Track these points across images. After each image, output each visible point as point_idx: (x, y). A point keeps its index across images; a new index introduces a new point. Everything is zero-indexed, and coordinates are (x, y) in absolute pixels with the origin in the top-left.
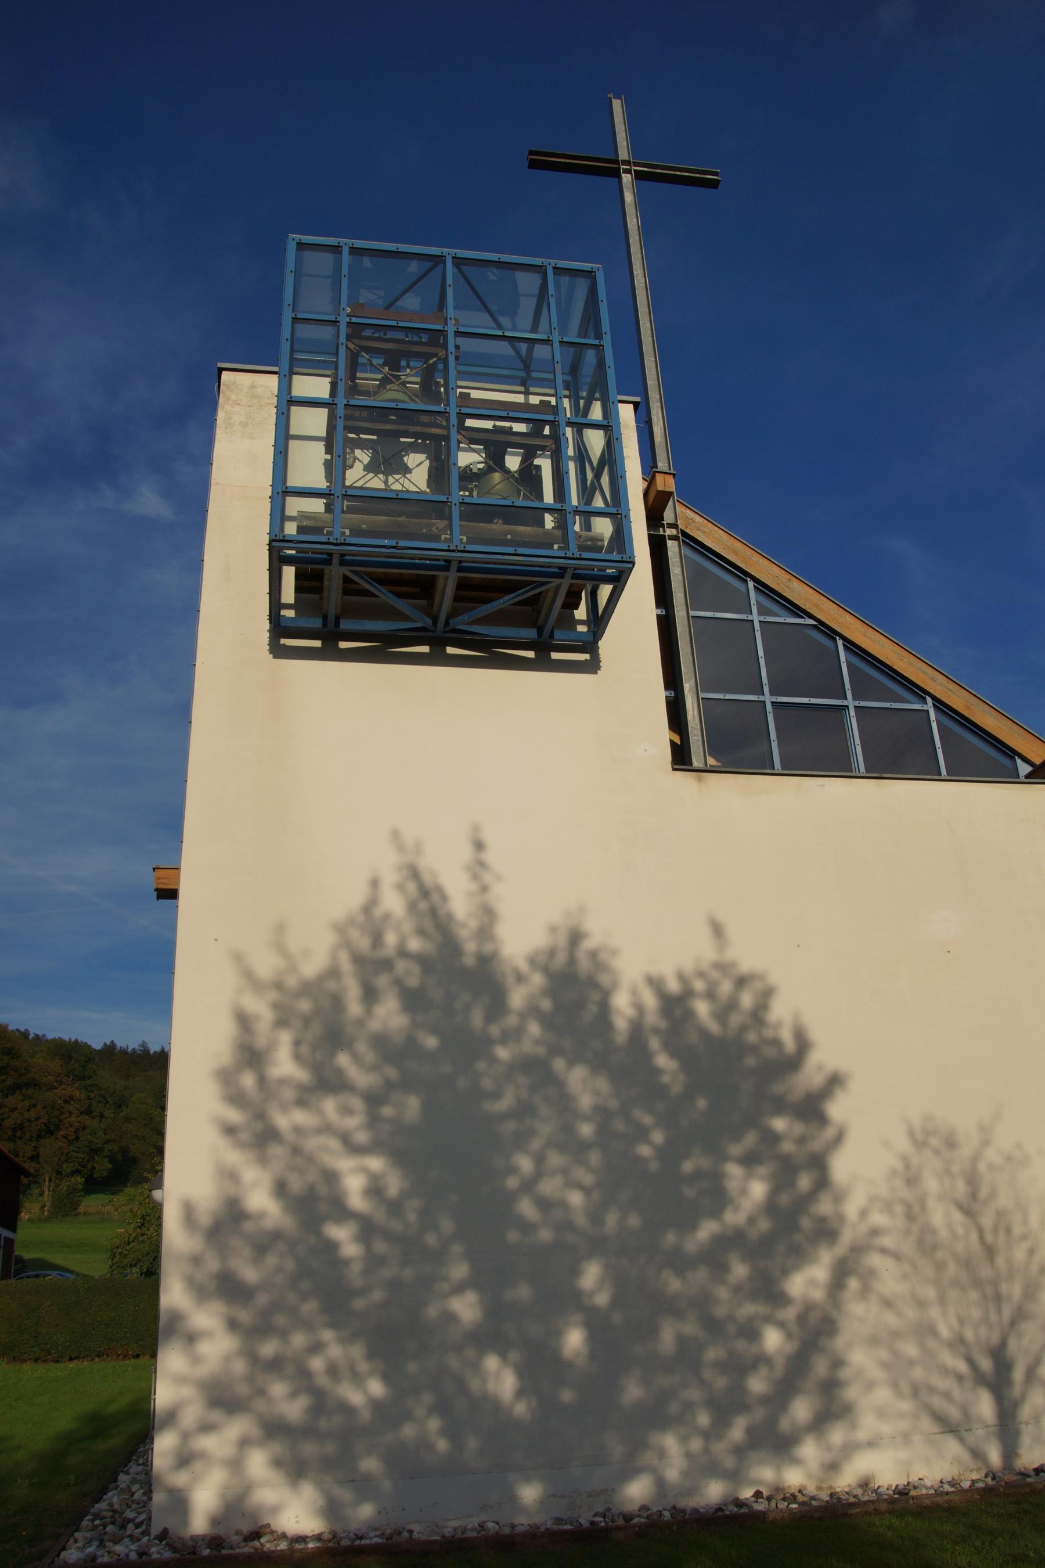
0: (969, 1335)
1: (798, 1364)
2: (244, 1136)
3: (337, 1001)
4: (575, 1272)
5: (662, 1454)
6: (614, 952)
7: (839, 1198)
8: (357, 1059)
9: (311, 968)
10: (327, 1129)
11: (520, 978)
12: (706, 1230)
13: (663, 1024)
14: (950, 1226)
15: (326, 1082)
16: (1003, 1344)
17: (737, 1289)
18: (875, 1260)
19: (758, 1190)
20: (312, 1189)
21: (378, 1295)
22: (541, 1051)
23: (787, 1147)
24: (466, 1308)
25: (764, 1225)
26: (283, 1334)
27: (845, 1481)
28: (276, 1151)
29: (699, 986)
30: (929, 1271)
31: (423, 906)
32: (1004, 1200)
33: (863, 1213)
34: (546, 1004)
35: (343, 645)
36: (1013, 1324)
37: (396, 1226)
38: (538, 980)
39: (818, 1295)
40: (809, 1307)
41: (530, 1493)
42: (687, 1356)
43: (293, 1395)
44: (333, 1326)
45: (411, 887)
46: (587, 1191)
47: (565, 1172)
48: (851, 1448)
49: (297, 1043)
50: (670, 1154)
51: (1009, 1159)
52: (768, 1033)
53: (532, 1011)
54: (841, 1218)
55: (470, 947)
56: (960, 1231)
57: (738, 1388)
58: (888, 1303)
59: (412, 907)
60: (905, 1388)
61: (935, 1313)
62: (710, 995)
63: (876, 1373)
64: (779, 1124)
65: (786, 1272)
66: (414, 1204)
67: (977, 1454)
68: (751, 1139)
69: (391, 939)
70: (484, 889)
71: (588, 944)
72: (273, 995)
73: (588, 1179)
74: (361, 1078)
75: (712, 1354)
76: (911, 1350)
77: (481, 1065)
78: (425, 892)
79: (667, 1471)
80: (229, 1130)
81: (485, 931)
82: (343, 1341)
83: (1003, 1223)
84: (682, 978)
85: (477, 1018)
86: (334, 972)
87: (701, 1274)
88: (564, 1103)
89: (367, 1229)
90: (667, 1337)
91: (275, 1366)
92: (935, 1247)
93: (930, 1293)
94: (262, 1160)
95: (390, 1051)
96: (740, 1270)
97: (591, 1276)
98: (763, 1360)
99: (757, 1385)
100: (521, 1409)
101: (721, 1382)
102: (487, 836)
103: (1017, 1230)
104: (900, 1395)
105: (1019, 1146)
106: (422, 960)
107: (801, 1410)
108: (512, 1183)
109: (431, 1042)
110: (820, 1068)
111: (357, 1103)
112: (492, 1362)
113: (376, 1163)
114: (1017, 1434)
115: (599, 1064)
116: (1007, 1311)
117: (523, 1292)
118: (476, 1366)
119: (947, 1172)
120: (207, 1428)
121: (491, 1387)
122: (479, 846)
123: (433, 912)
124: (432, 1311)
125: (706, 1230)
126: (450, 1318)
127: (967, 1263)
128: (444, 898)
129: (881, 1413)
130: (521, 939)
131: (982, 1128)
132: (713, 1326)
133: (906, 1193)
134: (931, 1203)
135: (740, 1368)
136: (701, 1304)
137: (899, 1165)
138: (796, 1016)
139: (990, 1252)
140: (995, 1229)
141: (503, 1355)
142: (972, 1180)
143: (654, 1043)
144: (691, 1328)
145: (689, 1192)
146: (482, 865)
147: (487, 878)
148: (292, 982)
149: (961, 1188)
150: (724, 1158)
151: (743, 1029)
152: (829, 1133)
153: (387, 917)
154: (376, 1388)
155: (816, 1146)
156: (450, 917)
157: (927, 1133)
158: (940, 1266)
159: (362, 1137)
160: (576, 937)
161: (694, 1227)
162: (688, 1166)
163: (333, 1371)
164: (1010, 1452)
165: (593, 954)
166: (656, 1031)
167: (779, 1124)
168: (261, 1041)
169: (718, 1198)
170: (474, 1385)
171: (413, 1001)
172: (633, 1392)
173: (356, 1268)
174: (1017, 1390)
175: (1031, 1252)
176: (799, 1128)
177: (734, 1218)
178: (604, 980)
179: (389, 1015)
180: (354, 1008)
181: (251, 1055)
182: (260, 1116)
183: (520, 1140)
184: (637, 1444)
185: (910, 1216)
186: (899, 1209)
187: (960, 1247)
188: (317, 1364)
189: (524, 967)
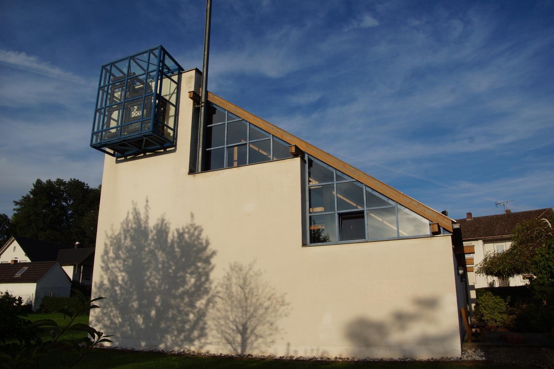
0: (237, 320)
1: (196, 322)
2: (104, 269)
3: (120, 239)
4: (155, 298)
5: (167, 339)
6: (170, 224)
7: (211, 283)
8: (122, 253)
9: (116, 233)
10: (117, 267)
11: (152, 232)
12: (181, 290)
13: (178, 241)
14: (237, 292)
15: (117, 257)
16: (246, 323)
17: (185, 304)
18: (217, 299)
19: (193, 280)
20: (113, 279)
21: (122, 301)
22: (154, 248)
23: (200, 270)
24: (135, 304)
25: (193, 289)
26: (107, 308)
27: (203, 351)
28: (109, 272)
29: (186, 230)
30: (229, 303)
31: (136, 217)
32: (253, 285)
33: (216, 287)
34: (155, 237)
35: (128, 157)
36: (249, 318)
37: (126, 287)
38: (155, 231)
39: (203, 307)
40: (200, 309)
41: (143, 344)
42: (174, 318)
43: (108, 320)
44: (115, 307)
45: (134, 213)
46: (159, 280)
47: (155, 276)
48: (206, 344)
49: (113, 249)
50: (176, 272)
51: (256, 274)
52: (200, 241)
53: (153, 239)
54: (211, 288)
55: (143, 225)
56: (239, 293)
57: (183, 327)
58: (218, 310)
59: (134, 218)
60: (220, 331)
61: (229, 313)
62: (188, 233)
63: (213, 327)
64: (199, 264)
65: (196, 301)
66: (129, 282)
67: (235, 350)
68: (193, 268)
69: (130, 225)
70: (147, 211)
71: (165, 222)
72: (110, 239)
73: (159, 277)
74: (123, 256)
75: (179, 318)
76: (222, 322)
77: (143, 252)
78: (137, 214)
79: (168, 343)
80: (102, 268)
81: (146, 222)
82: (116, 310)
83: (251, 292)
84: (183, 229)
85: (143, 241)
86: (120, 234)
87: (178, 300)
88: (156, 259)
89: (121, 288)
90: (170, 314)
91: (105, 314)
92: (232, 297)
93: (229, 308)
94: (107, 274)
95: (129, 250)
96: (186, 300)
97: (158, 299)
98: (189, 321)
99: (187, 326)
100: (143, 327)
101: (180, 325)
102: (149, 199)
103: (255, 294)
104: (218, 333)
105: (259, 270)
106: (135, 229)
107: (196, 333)
108: (146, 278)
109: (135, 247)
110: (211, 250)
111: (122, 261)
112: (139, 316)
113: (123, 274)
114: (246, 346)
115: (164, 251)
116: (248, 315)
117: (145, 302)
118: (136, 317)
119: (239, 277)
120: (96, 325)
121: (138, 321)
122: (147, 201)
123: (138, 218)
124: (130, 305)
125: (181, 290)
126: (133, 306)
127: (240, 302)
128: (140, 215)
129: (213, 337)
130: (152, 223)
131: (250, 265)
132: (180, 312)
133: (227, 283)
134: (233, 285)
135: (184, 322)
136: (178, 307)
137: (226, 275)
138: (207, 236)
139: (246, 299)
140: (249, 293)
141: (140, 315)
142: (245, 279)
143: (176, 245)
144: (175, 312)
145: (178, 281)
146: (147, 205)
147: (148, 209)
148: (113, 236)
149: (242, 281)
150: (187, 273)
151: (195, 240)
152: (211, 266)
153: (130, 220)
154: (120, 320)
155: (207, 270)
156: (140, 219)
157: (235, 266)
158: (233, 302)
159: (122, 268)
160: (163, 220)
161: (178, 289)
162: (179, 275)
163: (114, 316)
164: (243, 350)
165: (166, 224)
166: (176, 242)
167: (199, 264)
168: (108, 250)
169: (184, 282)
170: (136, 321)
171: (133, 239)
172: (163, 325)
173: (119, 295)
174: (248, 336)
175: (258, 300)
176: (204, 265)
177: (187, 287)
178: (167, 230)
179: (128, 242)
180: (123, 241)
181: (106, 252)
182: (107, 265)
183: (148, 269)
184: (163, 337)
185: (227, 289)
186: (225, 286)
187: (239, 297)
188: (112, 314)
189: (153, 229)
